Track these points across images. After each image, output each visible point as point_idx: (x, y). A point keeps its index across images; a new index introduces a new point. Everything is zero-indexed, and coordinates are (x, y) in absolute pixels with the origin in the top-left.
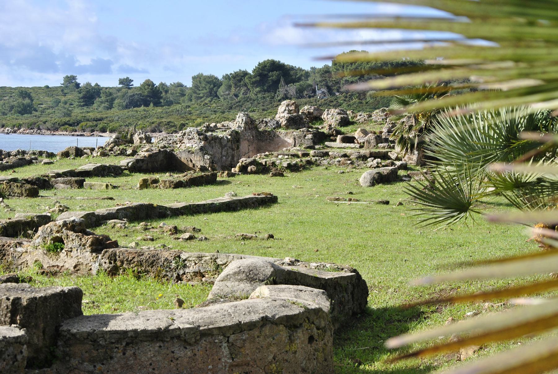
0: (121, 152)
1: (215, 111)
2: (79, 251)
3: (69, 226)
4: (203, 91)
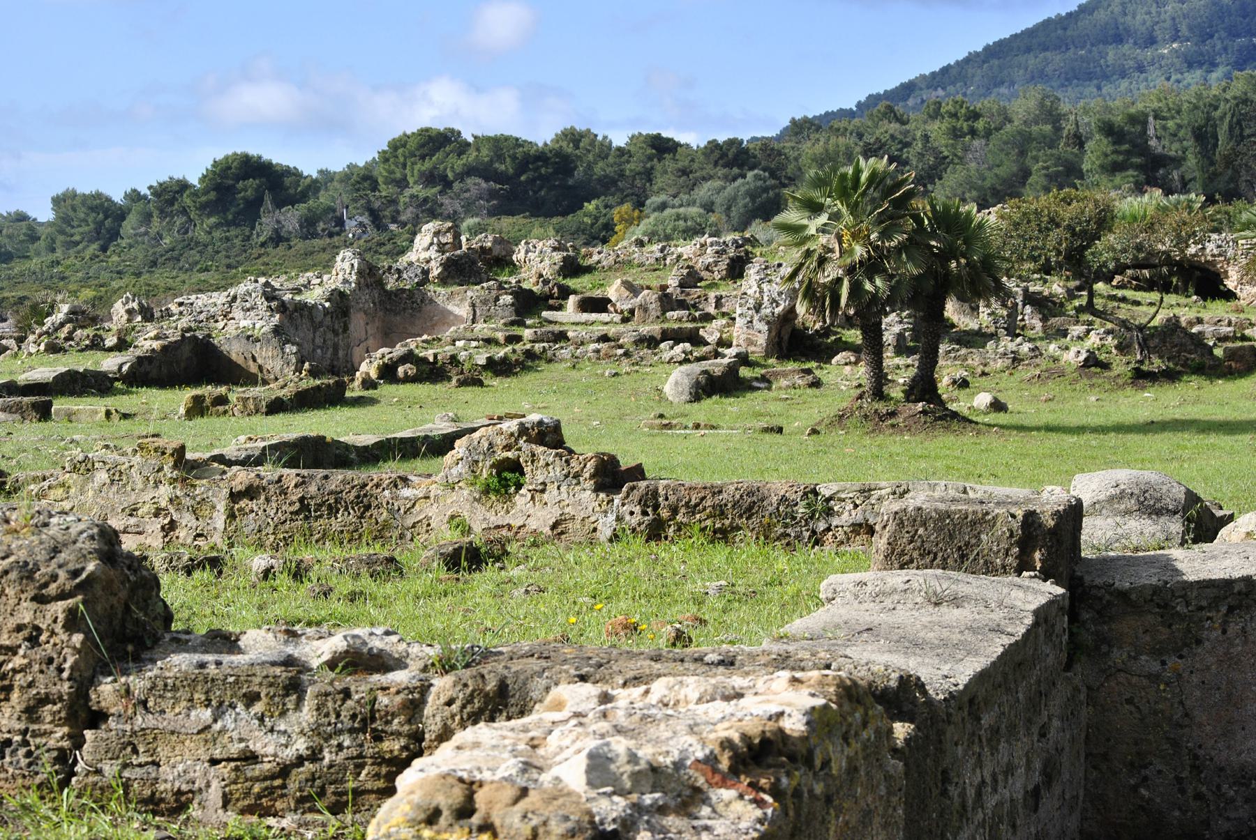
0: (92, 341)
1: (119, 273)
2: (562, 489)
3: (533, 433)
4: (81, 230)
